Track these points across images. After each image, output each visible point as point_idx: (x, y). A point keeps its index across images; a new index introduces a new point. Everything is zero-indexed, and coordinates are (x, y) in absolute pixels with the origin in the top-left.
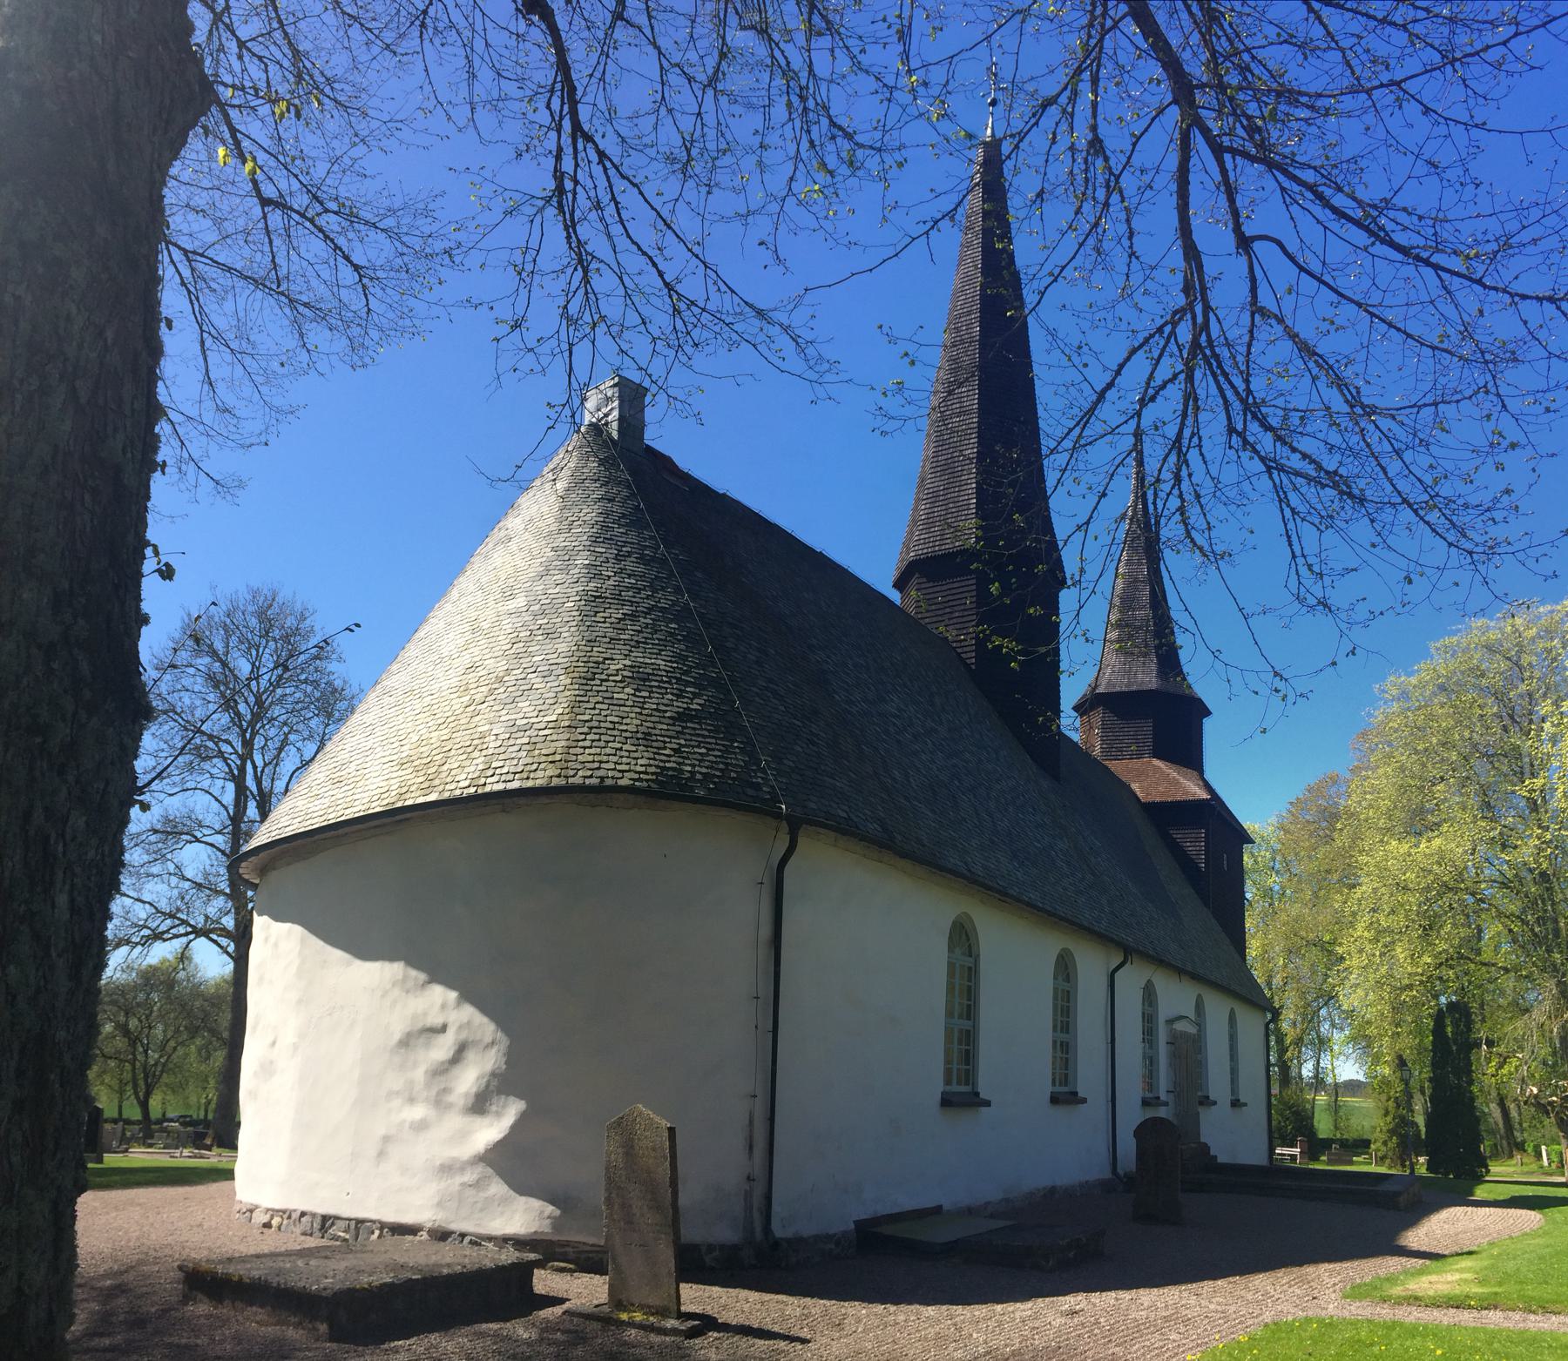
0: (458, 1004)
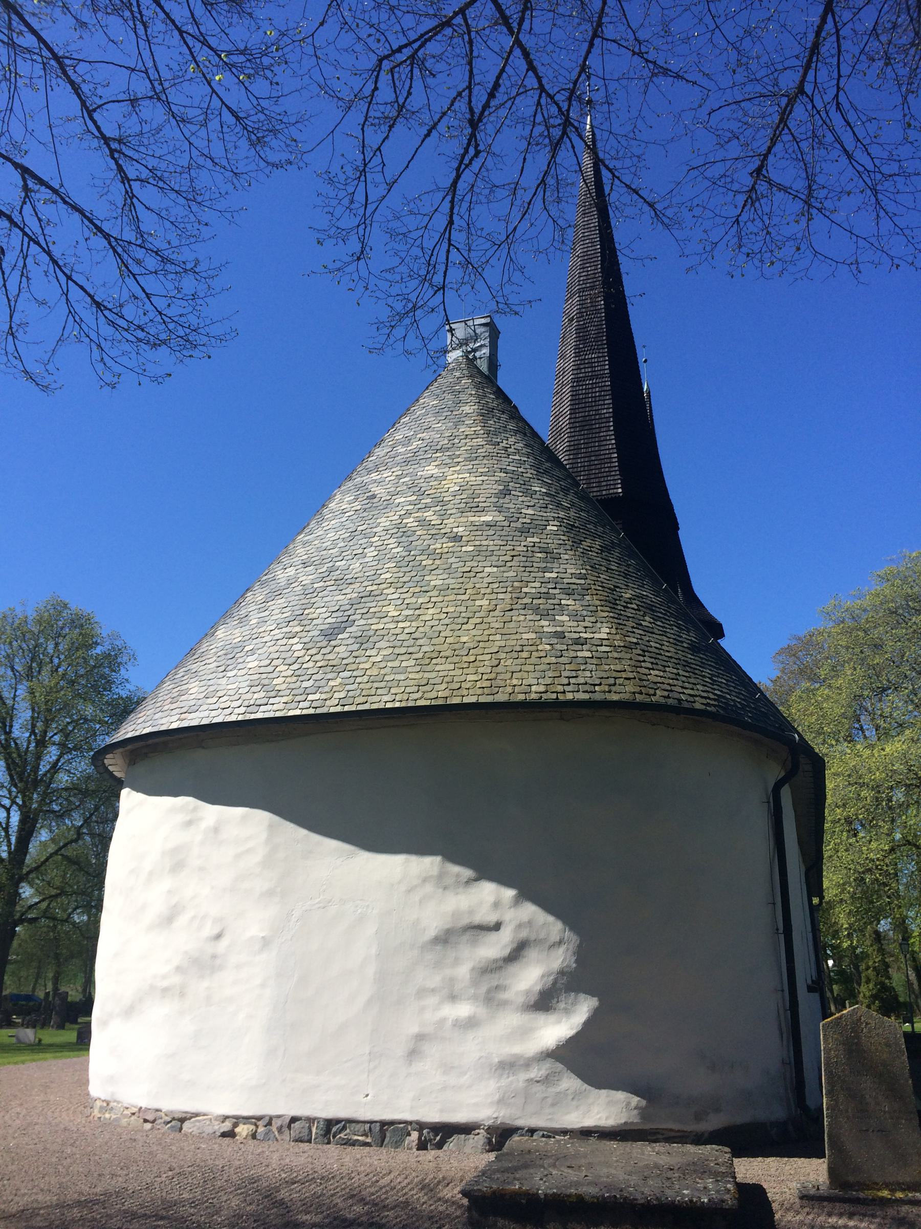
0: (517, 901)
